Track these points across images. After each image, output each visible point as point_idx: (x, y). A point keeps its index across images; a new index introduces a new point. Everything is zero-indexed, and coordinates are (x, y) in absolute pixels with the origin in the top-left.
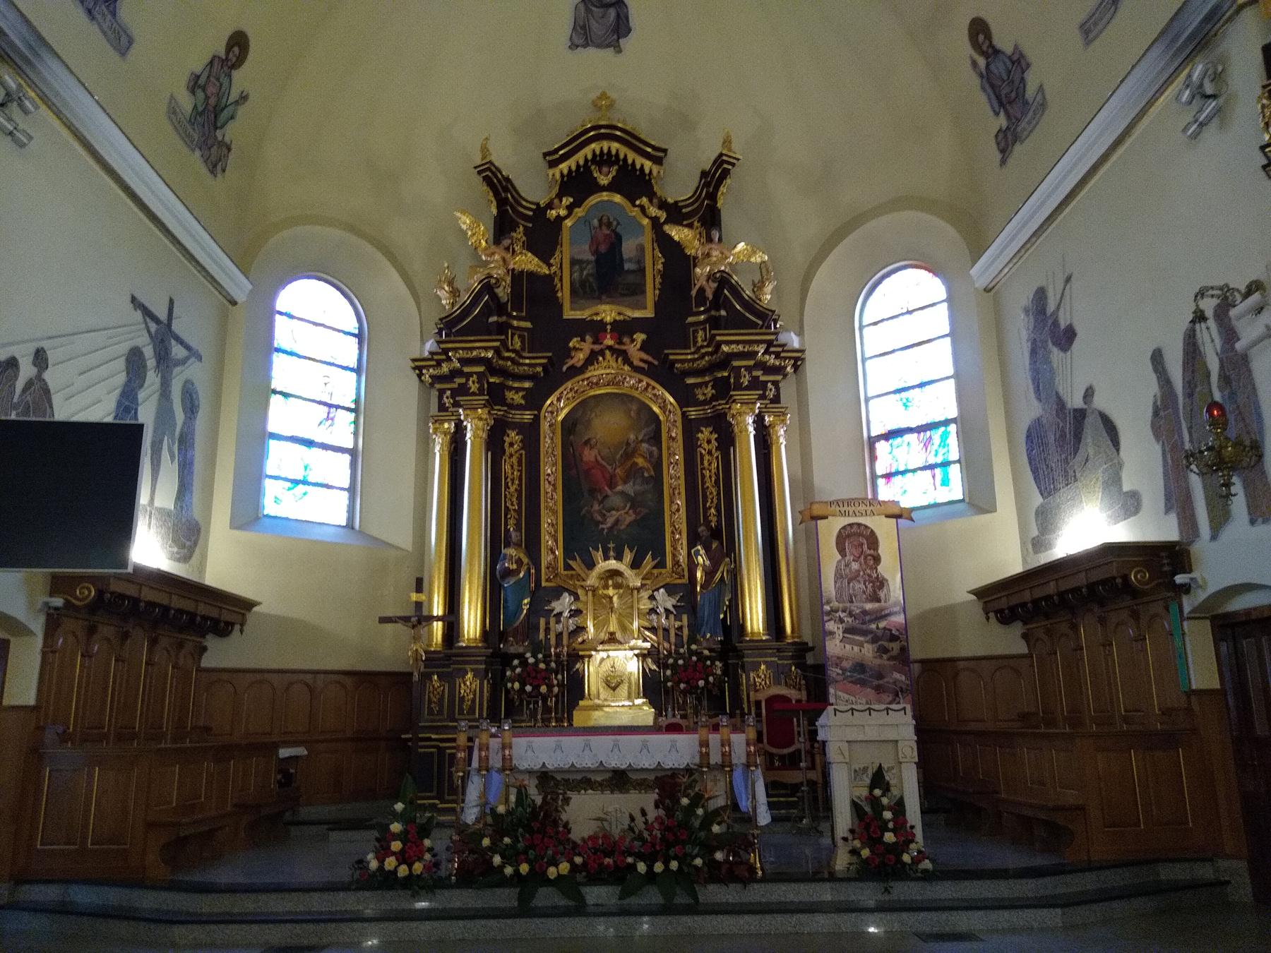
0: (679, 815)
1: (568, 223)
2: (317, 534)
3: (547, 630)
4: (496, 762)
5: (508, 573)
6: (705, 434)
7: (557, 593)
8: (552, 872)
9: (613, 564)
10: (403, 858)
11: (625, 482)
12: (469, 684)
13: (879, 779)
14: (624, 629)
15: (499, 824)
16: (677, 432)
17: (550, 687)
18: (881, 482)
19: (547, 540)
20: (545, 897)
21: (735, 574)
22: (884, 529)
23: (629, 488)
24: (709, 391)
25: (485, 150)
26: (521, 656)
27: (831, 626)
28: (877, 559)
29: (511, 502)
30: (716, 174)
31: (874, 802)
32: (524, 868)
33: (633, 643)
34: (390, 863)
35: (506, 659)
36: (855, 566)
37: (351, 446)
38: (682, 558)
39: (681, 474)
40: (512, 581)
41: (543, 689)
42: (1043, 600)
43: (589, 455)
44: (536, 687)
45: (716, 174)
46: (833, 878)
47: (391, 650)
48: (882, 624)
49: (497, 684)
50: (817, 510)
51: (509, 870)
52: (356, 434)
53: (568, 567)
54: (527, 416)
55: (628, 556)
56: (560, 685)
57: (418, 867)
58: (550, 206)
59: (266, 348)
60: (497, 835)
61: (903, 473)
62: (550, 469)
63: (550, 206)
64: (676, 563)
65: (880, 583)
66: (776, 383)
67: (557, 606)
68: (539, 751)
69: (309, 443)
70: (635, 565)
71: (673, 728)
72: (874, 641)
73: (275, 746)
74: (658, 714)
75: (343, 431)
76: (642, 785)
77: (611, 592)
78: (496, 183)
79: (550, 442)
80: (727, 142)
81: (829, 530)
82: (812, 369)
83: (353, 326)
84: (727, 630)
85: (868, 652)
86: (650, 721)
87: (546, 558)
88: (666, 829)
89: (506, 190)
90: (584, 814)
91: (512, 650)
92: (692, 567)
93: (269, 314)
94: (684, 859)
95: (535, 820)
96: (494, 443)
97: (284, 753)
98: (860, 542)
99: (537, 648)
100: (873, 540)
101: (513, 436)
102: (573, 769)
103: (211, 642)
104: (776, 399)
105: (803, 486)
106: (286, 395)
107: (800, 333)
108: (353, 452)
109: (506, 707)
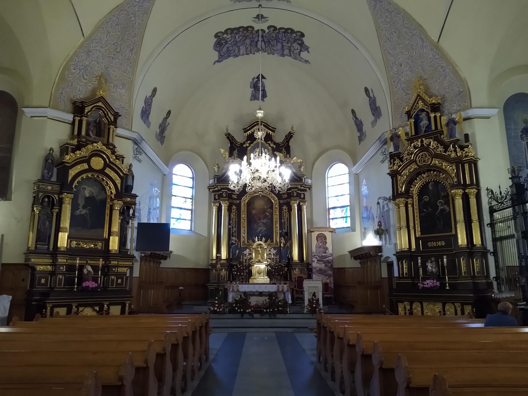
0: (273, 300)
1: (249, 148)
2: (184, 233)
3: (243, 259)
4: (236, 290)
5: (233, 244)
6: (285, 207)
7: (245, 249)
8: (247, 311)
9: (260, 242)
10: (218, 308)
11: (263, 219)
12: (224, 272)
13: (314, 295)
14: (262, 258)
15: (236, 302)
16: (277, 206)
17: (244, 273)
18: (331, 220)
19: (242, 235)
20: (246, 316)
21: (291, 245)
22: (328, 235)
23: (264, 221)
24: (286, 196)
25: (227, 129)
26: (236, 265)
27: (314, 259)
28: (326, 243)
29: (233, 222)
30: (289, 136)
31: (312, 299)
32: (242, 310)
33: (265, 262)
34: (216, 309)
35: (232, 266)
36: (321, 244)
37: (191, 208)
38: (278, 240)
39: (278, 218)
40: (234, 246)
41: (242, 274)
42: (364, 255)
43: (254, 212)
44: (240, 274)
45: (289, 136)
46: (303, 313)
47: (202, 264)
48: (327, 259)
49: (230, 272)
50: (312, 230)
51: (239, 310)
52: (192, 205)
53: (248, 242)
54: (238, 202)
55: (264, 239)
56: (246, 273)
57: (221, 310)
58: (244, 143)
59: (171, 184)
60: (236, 305)
61: (336, 218)
62: (244, 216)
63: (244, 143)
64: (276, 241)
65: (327, 249)
66: (303, 194)
67: (245, 252)
68: (244, 288)
69: (181, 208)
70: (266, 242)
71: (273, 284)
72: (324, 263)
73: (178, 287)
74: (271, 281)
75: (189, 204)
76: (265, 295)
77: (259, 249)
78: (229, 137)
79: (243, 208)
80: (292, 128)
81: (314, 235)
82: (314, 189)
83: (191, 175)
84: (289, 259)
85: (323, 266)
86: (269, 282)
87: (242, 240)
88: (270, 303)
89: (232, 139)
90: (253, 301)
91: (234, 264)
92: (280, 242)
93: (171, 174)
94: (273, 309)
95: (244, 300)
96: (229, 210)
97: (180, 288)
98: (322, 238)
99: (241, 263)
100: (325, 238)
101: (234, 207)
102: (251, 292)
103: (162, 261)
104: (304, 198)
105: (310, 222)
106: (175, 196)
107: (311, 179)
108: (191, 210)
109: (232, 278)
